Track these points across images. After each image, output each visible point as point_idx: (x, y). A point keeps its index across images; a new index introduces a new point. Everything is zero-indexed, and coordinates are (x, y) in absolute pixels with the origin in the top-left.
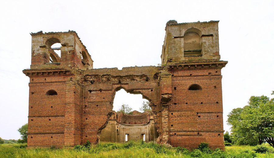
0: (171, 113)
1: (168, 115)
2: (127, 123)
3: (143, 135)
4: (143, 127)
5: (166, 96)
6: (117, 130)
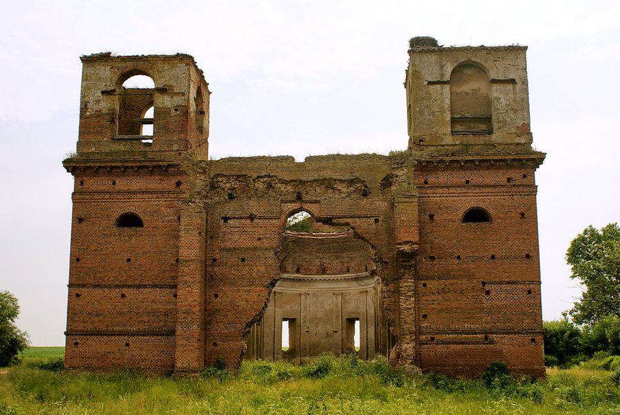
0: (423, 282)
1: (413, 290)
2: (289, 268)
3: (351, 322)
5: (406, 248)
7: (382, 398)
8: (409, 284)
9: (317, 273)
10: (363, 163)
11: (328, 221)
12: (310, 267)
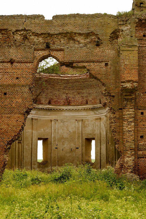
0: (141, 111)
1: (133, 117)
2: (43, 101)
3: (89, 141)
5: (128, 85)
7: (105, 198)
8: (130, 112)
9: (64, 105)
10: (96, 21)
11: (70, 65)
12: (58, 100)
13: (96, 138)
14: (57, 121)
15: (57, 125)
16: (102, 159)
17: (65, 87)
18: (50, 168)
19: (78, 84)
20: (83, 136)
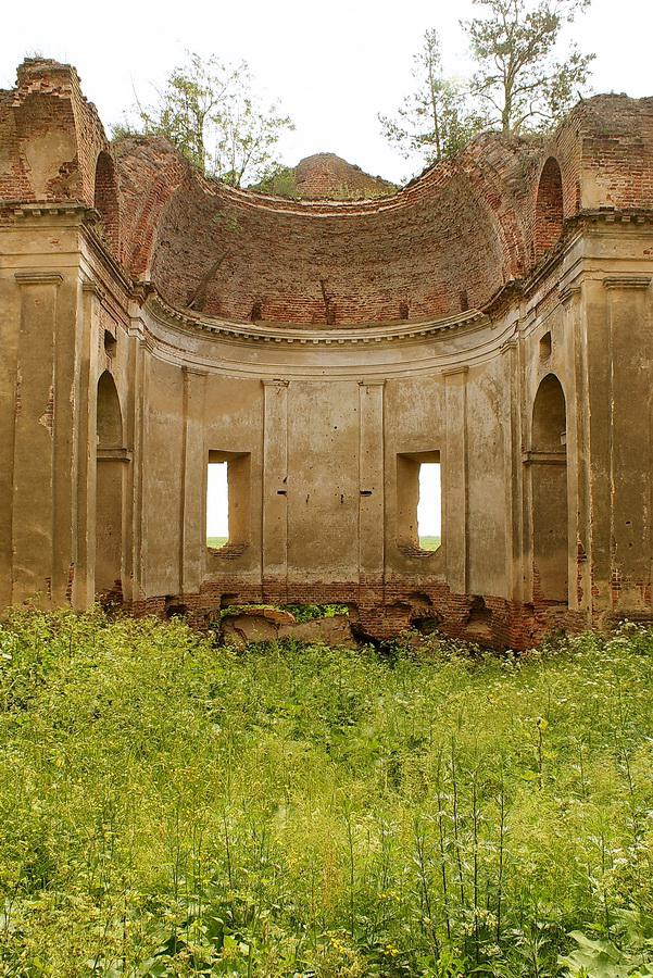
3: (410, 463)
4: (424, 363)
6: (107, 382)
9: (313, 324)
13: (446, 451)
14: (287, 385)
15: (285, 402)
16: (474, 535)
17: (319, 253)
18: (259, 571)
19: (368, 237)
20: (389, 444)
